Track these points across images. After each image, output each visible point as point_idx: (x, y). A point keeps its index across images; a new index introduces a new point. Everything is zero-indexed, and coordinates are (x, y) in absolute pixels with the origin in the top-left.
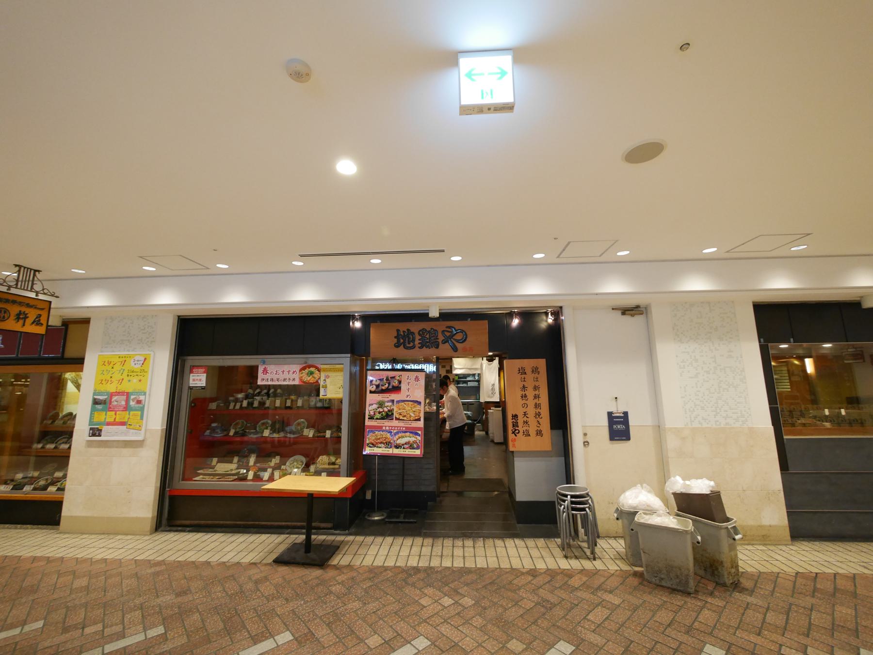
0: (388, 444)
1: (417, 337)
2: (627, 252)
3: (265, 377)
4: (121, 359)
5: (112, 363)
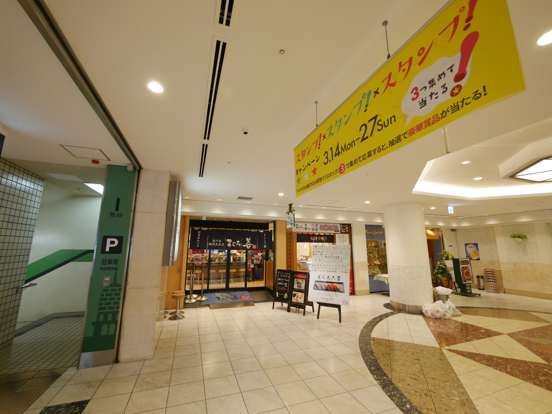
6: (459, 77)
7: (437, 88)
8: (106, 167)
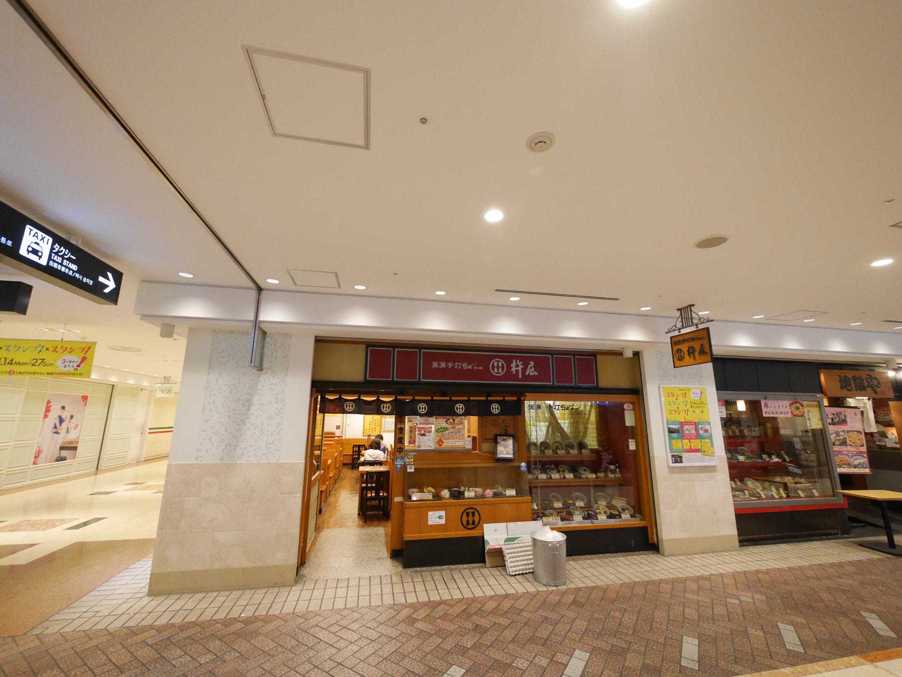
0: (849, 465)
1: (853, 382)
2: (364, 288)
3: (767, 410)
4: (682, 392)
5: (675, 395)
6: (78, 366)
7: (71, 364)
8: (400, 559)
